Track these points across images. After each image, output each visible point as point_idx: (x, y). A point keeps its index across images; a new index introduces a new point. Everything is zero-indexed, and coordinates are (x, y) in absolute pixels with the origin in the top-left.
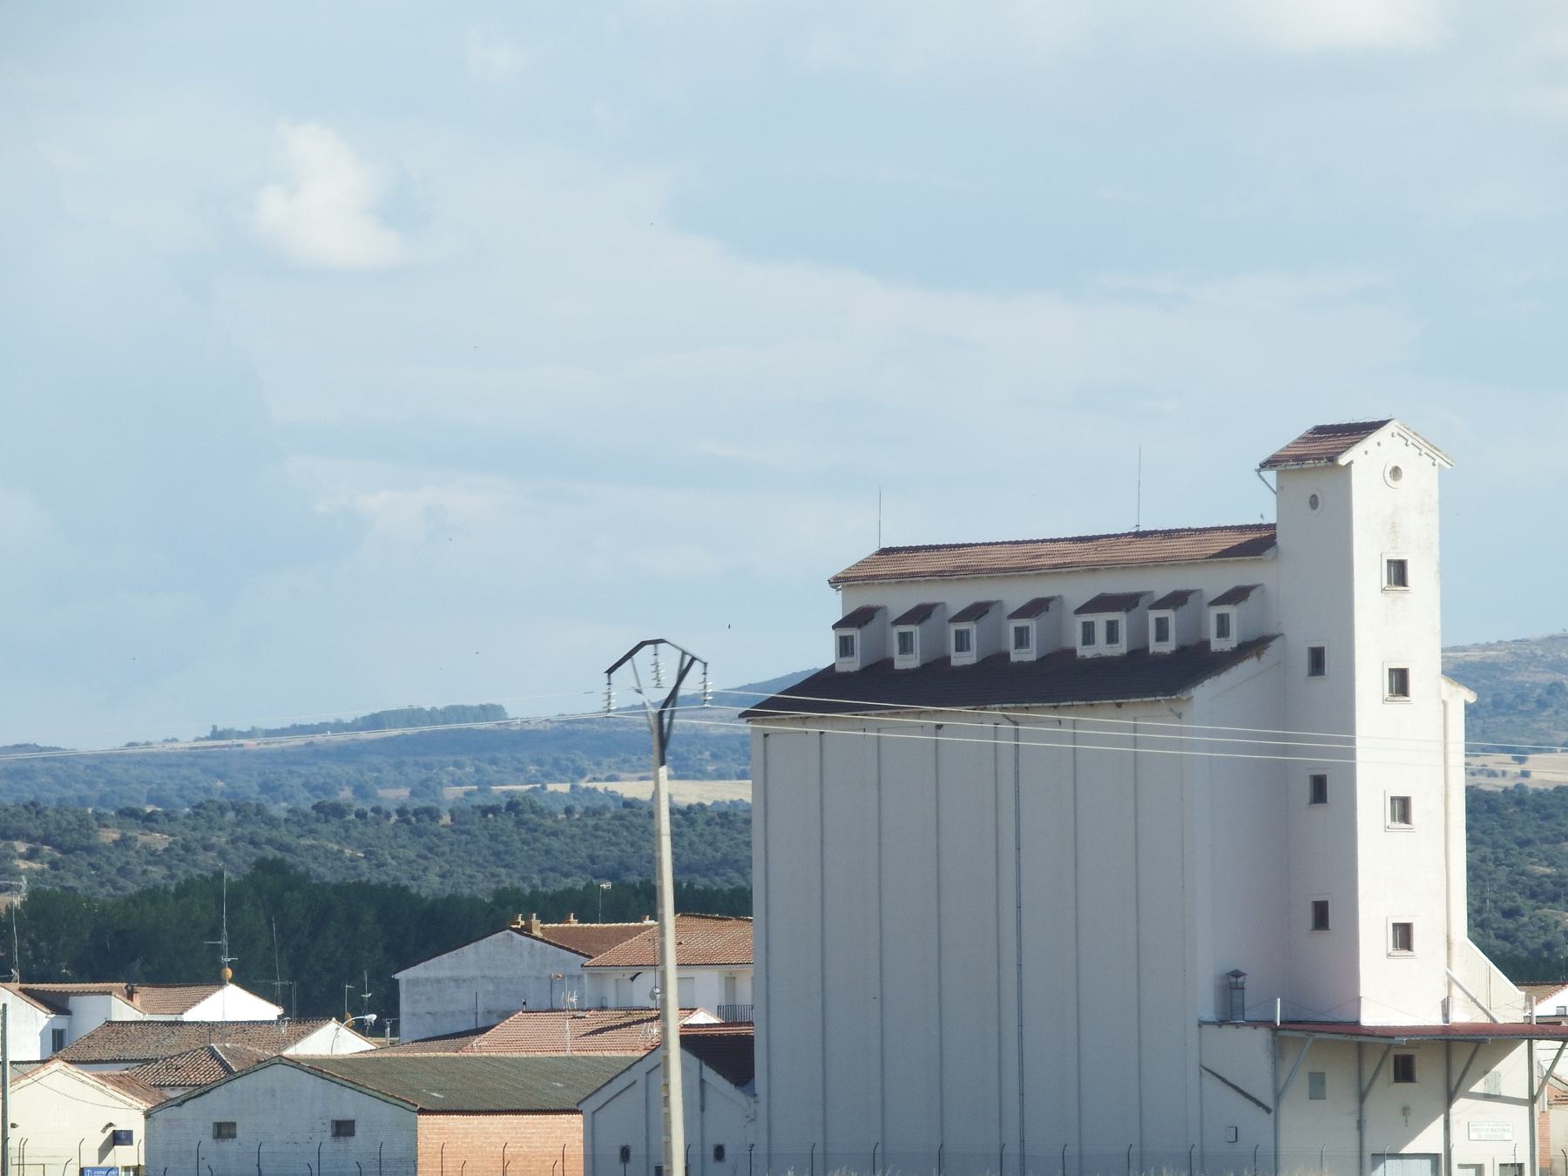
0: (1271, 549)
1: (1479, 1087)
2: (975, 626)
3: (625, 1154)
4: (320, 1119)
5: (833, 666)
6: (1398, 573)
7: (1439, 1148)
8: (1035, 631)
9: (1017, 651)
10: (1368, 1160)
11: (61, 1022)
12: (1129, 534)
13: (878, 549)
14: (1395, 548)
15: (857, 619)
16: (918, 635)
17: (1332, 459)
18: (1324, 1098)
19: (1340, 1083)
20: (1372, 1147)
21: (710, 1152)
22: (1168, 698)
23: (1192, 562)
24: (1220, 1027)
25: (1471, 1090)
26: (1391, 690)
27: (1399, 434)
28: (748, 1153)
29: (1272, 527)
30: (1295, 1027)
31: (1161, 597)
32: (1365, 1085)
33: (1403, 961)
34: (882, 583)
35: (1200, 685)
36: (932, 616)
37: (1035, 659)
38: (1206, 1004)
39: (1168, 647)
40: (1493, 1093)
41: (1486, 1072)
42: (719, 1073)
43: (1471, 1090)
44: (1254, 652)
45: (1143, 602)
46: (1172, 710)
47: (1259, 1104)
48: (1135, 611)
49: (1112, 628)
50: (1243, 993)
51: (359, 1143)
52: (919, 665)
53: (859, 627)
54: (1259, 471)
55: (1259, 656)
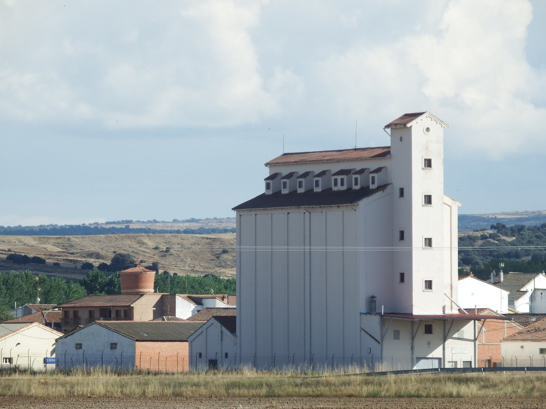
0: (389, 155)
1: (456, 335)
2: (304, 180)
3: (200, 355)
4: (107, 342)
5: (265, 193)
6: (428, 163)
7: (441, 356)
8: (272, 184)
9: (316, 188)
10: (415, 359)
11: (200, 308)
12: (353, 149)
13: (283, 154)
14: (427, 155)
15: (272, 177)
16: (321, 181)
17: (405, 125)
18: (399, 339)
19: (405, 335)
20: (416, 354)
21: (224, 355)
22: (351, 204)
23: (366, 159)
24: (376, 315)
25: (453, 337)
26: (425, 202)
27: (429, 117)
28: (215, 355)
29: (389, 147)
30: (396, 315)
31: (301, 174)
32: (414, 334)
33: (428, 293)
34: (305, 163)
35: (362, 200)
36: (293, 176)
37: (321, 191)
38: (363, 308)
39: (357, 187)
40: (461, 338)
41: (458, 331)
42: (227, 329)
43: (453, 337)
44: (381, 189)
45: (352, 172)
46: (352, 208)
47: (377, 341)
48: (349, 176)
49: (342, 180)
50: (375, 304)
51: (118, 351)
52: (271, 194)
53: (272, 180)
54: (384, 129)
55: (383, 191)
